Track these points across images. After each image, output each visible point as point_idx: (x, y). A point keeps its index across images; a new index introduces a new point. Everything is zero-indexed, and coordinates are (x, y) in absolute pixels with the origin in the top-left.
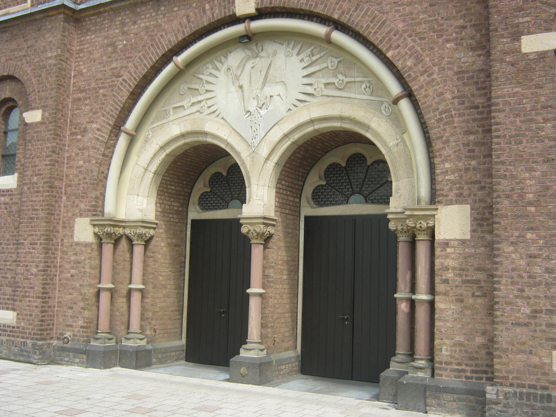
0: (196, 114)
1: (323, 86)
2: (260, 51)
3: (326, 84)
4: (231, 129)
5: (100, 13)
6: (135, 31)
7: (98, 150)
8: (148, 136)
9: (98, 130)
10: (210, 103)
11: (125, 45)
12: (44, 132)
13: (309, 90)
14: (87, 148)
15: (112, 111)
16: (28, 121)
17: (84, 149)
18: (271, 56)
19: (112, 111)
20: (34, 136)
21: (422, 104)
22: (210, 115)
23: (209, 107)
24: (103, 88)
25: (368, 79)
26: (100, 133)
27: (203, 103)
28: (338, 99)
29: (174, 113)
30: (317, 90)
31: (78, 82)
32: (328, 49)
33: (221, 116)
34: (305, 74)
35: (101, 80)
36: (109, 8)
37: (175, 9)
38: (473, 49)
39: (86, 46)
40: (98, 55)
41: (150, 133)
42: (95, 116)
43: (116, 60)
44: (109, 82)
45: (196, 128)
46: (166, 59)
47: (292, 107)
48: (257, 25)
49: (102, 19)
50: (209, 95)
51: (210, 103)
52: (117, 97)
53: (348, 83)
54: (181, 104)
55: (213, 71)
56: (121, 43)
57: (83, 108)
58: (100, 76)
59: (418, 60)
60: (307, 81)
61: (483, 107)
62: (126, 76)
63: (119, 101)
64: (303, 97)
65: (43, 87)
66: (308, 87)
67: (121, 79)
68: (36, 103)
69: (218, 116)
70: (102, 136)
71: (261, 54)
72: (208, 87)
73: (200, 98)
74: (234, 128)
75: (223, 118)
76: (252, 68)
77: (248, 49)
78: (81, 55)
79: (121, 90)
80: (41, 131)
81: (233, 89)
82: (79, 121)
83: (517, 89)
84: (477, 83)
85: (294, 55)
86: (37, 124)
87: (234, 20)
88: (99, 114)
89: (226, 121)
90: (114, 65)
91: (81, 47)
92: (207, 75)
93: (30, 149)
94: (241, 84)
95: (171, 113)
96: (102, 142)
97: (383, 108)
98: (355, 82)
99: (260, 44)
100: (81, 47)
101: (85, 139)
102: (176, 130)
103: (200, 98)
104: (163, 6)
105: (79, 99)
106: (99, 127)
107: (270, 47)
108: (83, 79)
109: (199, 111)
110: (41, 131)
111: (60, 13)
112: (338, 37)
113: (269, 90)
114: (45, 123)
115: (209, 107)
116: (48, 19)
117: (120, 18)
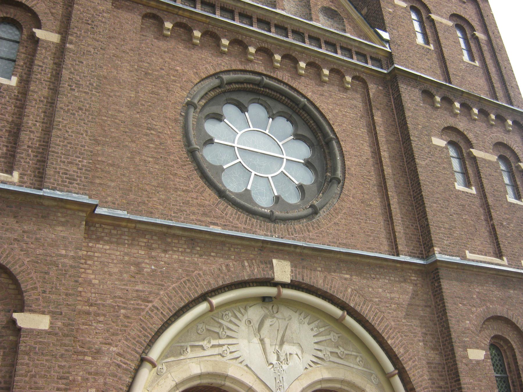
0: (217, 356)
1: (329, 354)
2: (275, 312)
3: (331, 353)
4: (256, 377)
5: (119, 226)
6: (166, 259)
7: (120, 378)
8: (162, 370)
9: (119, 354)
10: (232, 348)
11: (153, 271)
12: (54, 344)
13: (320, 354)
14: (103, 374)
15: (139, 337)
16: (20, 324)
17: (97, 374)
18: (287, 319)
19: (139, 337)
20: (35, 348)
21: (413, 381)
22: (232, 361)
23: (231, 353)
24: (124, 308)
25: (360, 355)
26: (123, 359)
27: (225, 347)
28: (341, 366)
29: (191, 351)
30: (326, 356)
31: (85, 292)
32: (329, 325)
33: (244, 363)
34: (316, 341)
35: (121, 298)
36: (134, 225)
37: (213, 254)
38: (433, 349)
39: (96, 254)
40: (116, 270)
41: (164, 367)
42: (114, 338)
43: (143, 283)
44: (133, 304)
45: (218, 370)
46: (204, 297)
47: (308, 367)
48: (287, 292)
49: (119, 232)
50: (230, 341)
51: (232, 348)
52: (146, 324)
53: (346, 354)
54: (201, 343)
55: (233, 319)
56: (148, 266)
57: (94, 324)
58: (118, 293)
59: (406, 351)
60: (317, 346)
61: (444, 388)
62: (157, 303)
63: (148, 327)
64: (315, 360)
65: (52, 288)
66: (319, 352)
67: (150, 305)
68: (39, 305)
69: (241, 363)
70: (125, 363)
71: (276, 315)
72: (229, 333)
73: (221, 342)
74: (259, 376)
75: (247, 366)
76: (271, 325)
77: (266, 308)
78: (89, 262)
79: (152, 317)
80: (49, 344)
81: (256, 340)
82: (88, 339)
83: (471, 381)
84: (438, 371)
85: (306, 323)
86: (40, 333)
87: (269, 282)
88: (119, 337)
89: (250, 368)
90: (140, 287)
91: (89, 253)
92: (227, 322)
93: (27, 364)
94: (262, 337)
95: (189, 349)
96: (126, 370)
97: (372, 378)
98: (351, 355)
99: (275, 307)
100: (89, 253)
101: (100, 363)
102: (196, 369)
103: (221, 342)
104: (198, 246)
105: (88, 313)
106: (121, 352)
107: (285, 312)
108: (93, 291)
109: (221, 354)
110: (49, 344)
111: (83, 211)
112: (350, 320)
113: (287, 348)
114: (56, 334)
115: (231, 353)
116: (61, 210)
117: (145, 240)
